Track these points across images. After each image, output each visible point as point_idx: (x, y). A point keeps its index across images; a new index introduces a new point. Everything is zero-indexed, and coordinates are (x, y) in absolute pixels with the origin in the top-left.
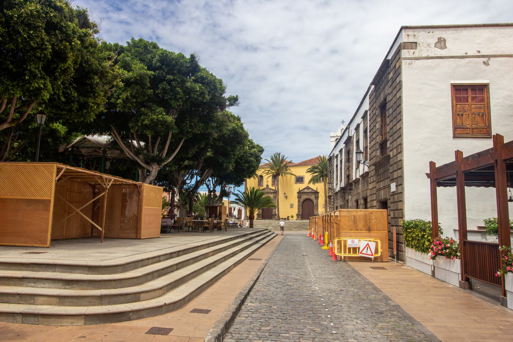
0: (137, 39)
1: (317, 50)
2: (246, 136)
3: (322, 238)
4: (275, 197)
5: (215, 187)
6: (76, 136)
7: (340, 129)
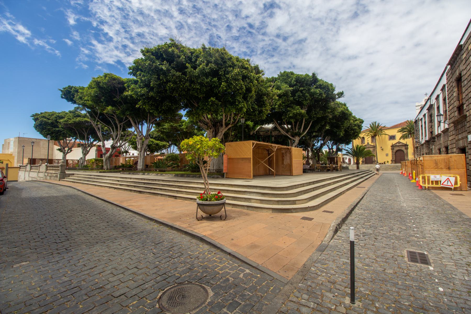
0: (282, 72)
1: (403, 47)
2: (351, 114)
3: (411, 175)
4: (374, 150)
5: (332, 146)
6: (258, 126)
7: (424, 100)
